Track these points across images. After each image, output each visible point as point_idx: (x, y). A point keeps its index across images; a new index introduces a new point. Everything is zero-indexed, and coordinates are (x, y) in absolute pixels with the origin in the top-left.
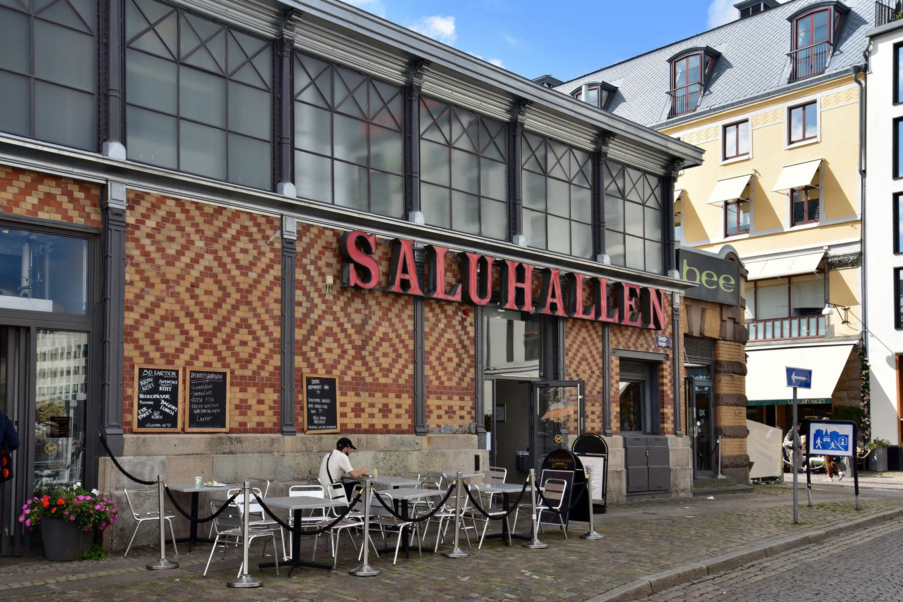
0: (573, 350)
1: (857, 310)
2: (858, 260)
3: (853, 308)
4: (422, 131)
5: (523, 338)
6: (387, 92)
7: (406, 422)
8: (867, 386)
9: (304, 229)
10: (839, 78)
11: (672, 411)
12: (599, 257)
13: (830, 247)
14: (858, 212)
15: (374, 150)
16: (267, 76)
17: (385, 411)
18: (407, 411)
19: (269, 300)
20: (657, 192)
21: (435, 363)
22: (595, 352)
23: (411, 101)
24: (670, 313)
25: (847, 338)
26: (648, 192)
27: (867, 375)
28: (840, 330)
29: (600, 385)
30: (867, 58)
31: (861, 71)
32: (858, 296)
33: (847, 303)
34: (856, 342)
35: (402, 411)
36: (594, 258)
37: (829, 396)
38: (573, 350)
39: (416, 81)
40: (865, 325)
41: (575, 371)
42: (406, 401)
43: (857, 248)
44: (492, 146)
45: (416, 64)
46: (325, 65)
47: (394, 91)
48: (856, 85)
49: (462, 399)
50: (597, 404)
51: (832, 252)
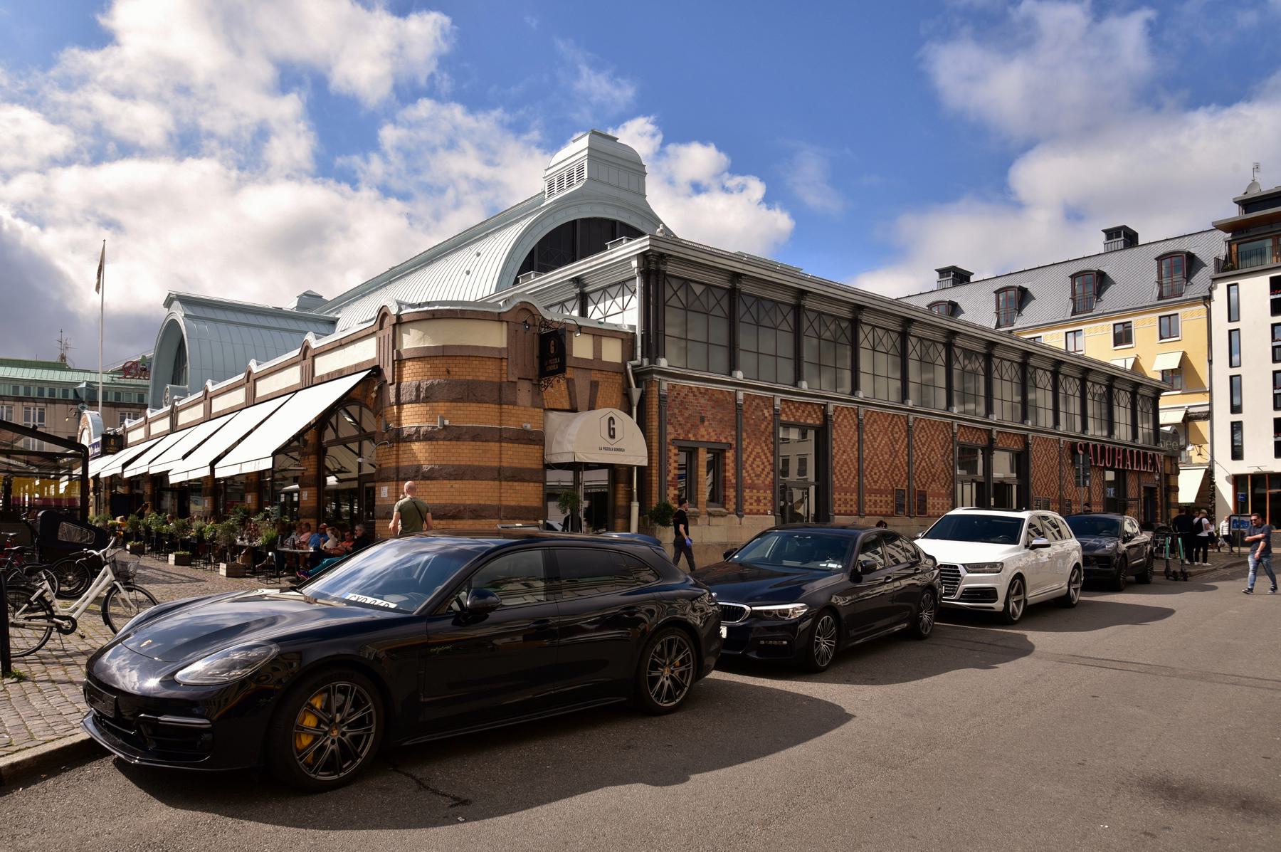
0: (749, 450)
1: (1207, 447)
2: (1208, 416)
3: (1204, 446)
4: (667, 298)
5: (1179, 486)
6: (786, 310)
7: (855, 509)
8: (1213, 495)
9: (747, 396)
10: (1193, 302)
11: (734, 494)
12: (950, 408)
13: (1189, 407)
14: (1207, 385)
15: (966, 385)
16: (727, 311)
17: (758, 501)
18: (746, 501)
19: (836, 448)
20: (1019, 373)
21: (749, 469)
22: (767, 451)
23: (734, 298)
24: (857, 422)
25: (1201, 464)
26: (1014, 373)
27: (1214, 488)
28: (1196, 459)
29: (856, 480)
30: (1210, 291)
31: (1207, 299)
32: (1207, 437)
33: (1200, 441)
34: (1207, 467)
35: (767, 501)
36: (948, 410)
37: (1193, 501)
38: (749, 450)
39: (860, 317)
40: (1212, 456)
41: (751, 466)
42: (855, 497)
43: (1207, 409)
44: (811, 328)
45: (802, 293)
46: (682, 282)
47: (723, 292)
48: (1203, 307)
49: (840, 494)
50: (854, 494)
51: (1191, 410)
